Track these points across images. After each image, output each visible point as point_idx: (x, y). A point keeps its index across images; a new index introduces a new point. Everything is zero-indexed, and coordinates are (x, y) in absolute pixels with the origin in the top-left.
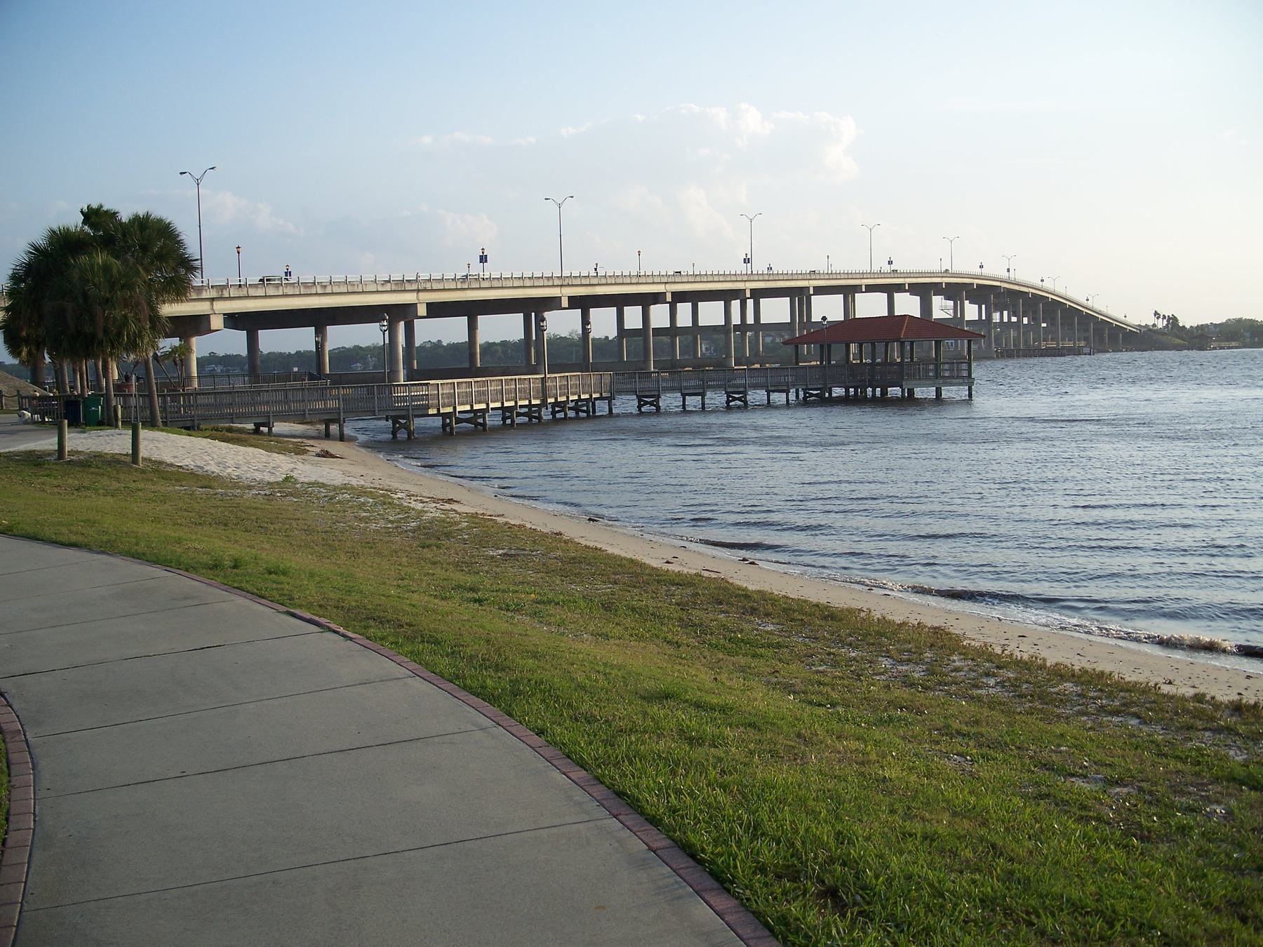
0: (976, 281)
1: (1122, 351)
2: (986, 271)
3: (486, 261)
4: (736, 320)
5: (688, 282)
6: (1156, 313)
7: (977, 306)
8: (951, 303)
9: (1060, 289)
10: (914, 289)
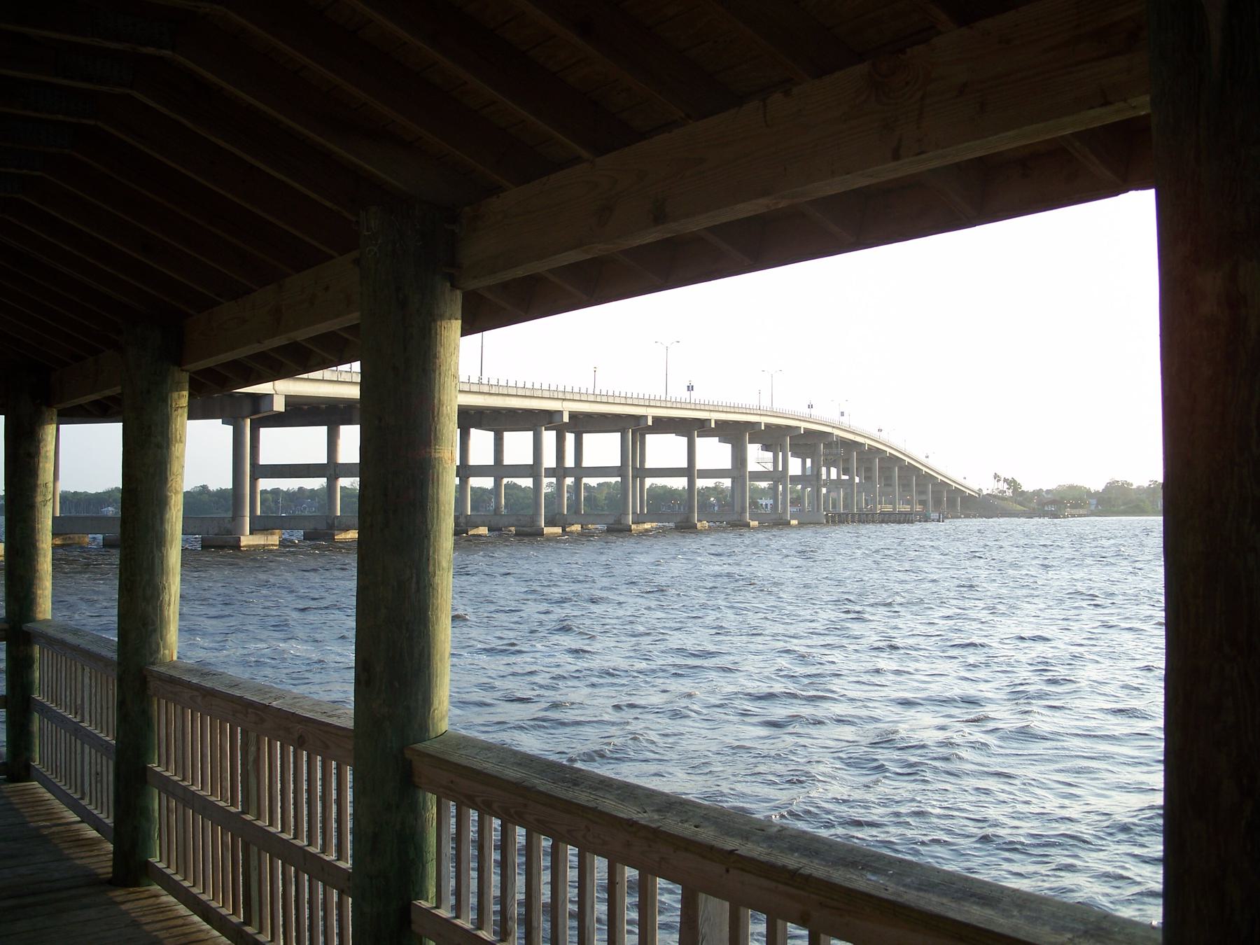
0: (803, 425)
1: (960, 517)
2: (817, 413)
4: (549, 461)
5: (550, 398)
7: (800, 460)
8: (770, 455)
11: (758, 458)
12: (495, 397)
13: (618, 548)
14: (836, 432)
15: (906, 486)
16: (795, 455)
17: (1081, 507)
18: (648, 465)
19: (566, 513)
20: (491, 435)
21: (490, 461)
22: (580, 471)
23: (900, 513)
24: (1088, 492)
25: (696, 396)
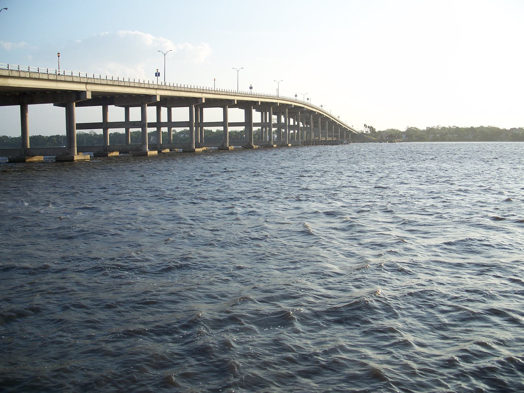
0: (293, 104)
3: (159, 76)
5: (198, 92)
6: (365, 125)
9: (328, 111)
10: (241, 104)
11: (257, 116)
12: (176, 92)
13: (249, 154)
14: (306, 107)
15: (330, 129)
16: (274, 114)
17: (400, 138)
18: (205, 121)
19: (161, 143)
20: (123, 109)
21: (155, 121)
22: (170, 124)
23: (329, 141)
24: (400, 132)
25: (254, 91)
